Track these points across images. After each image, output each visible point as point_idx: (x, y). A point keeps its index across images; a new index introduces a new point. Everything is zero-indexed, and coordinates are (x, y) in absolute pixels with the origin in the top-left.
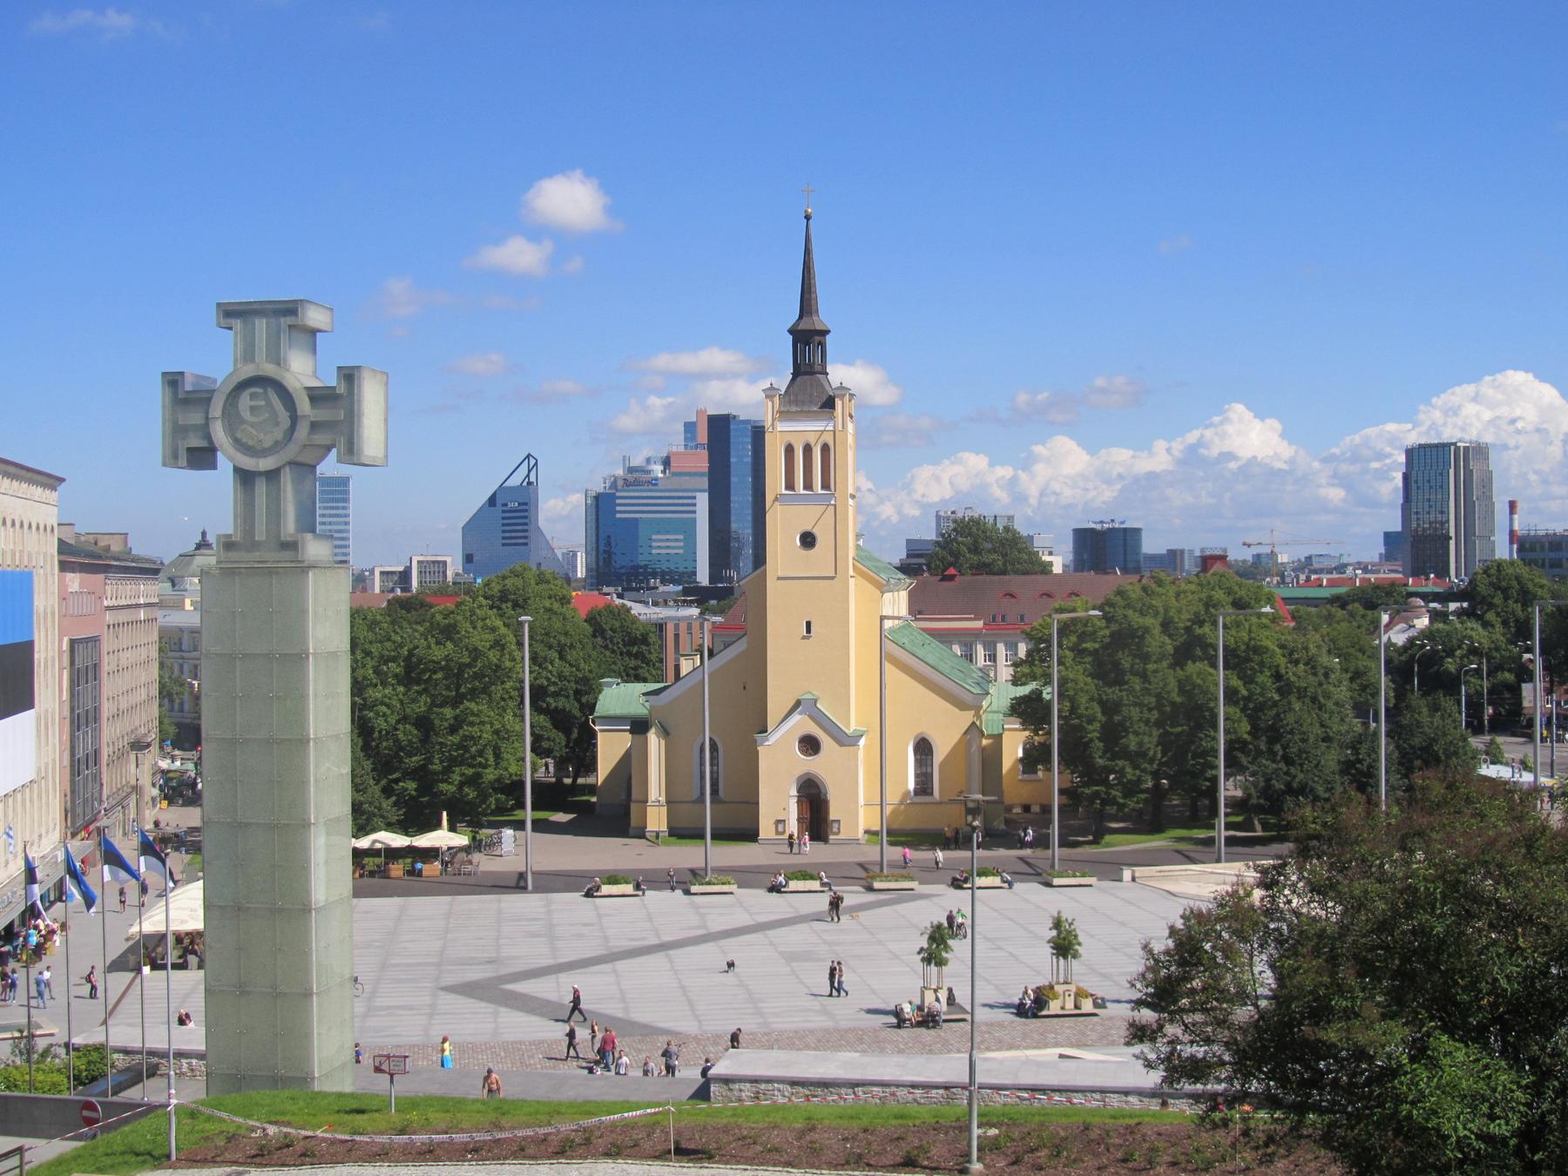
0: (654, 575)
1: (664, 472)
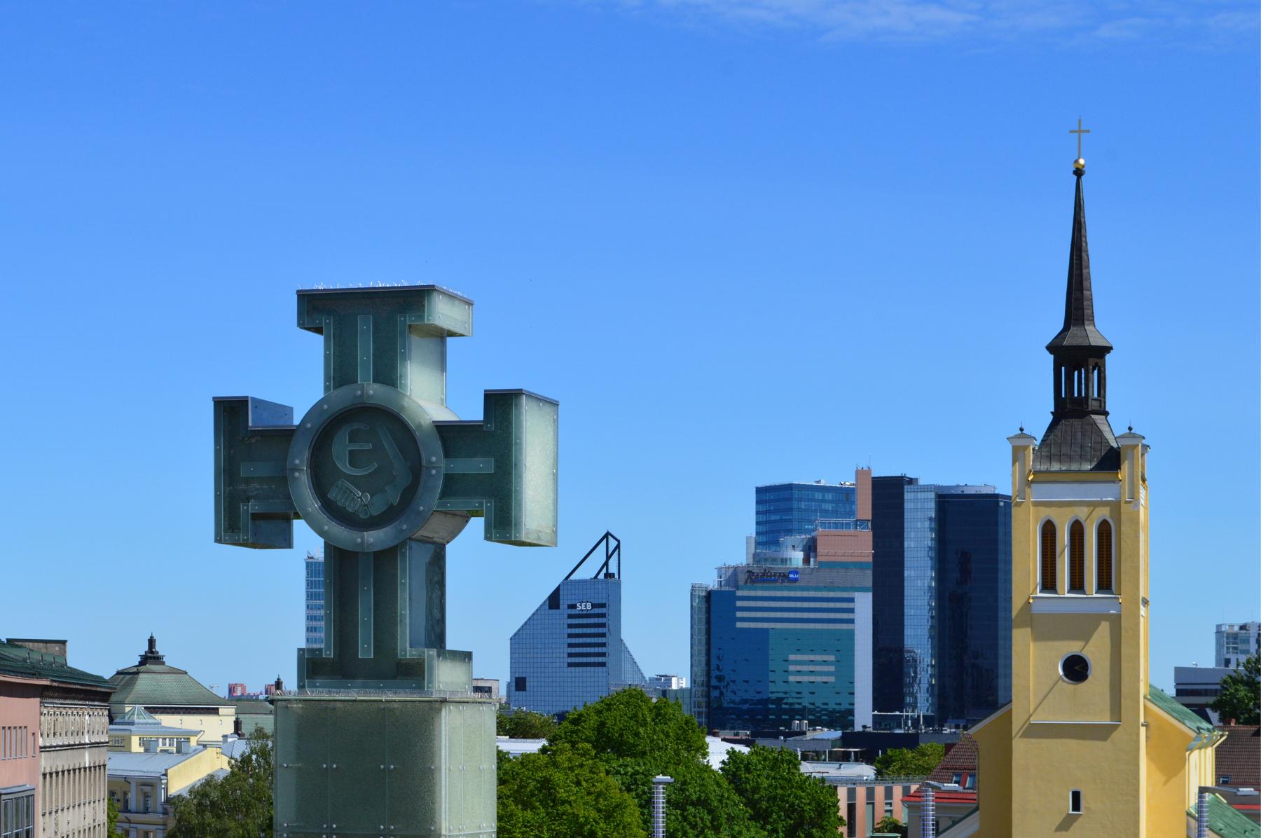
0: (802, 713)
1: (806, 560)
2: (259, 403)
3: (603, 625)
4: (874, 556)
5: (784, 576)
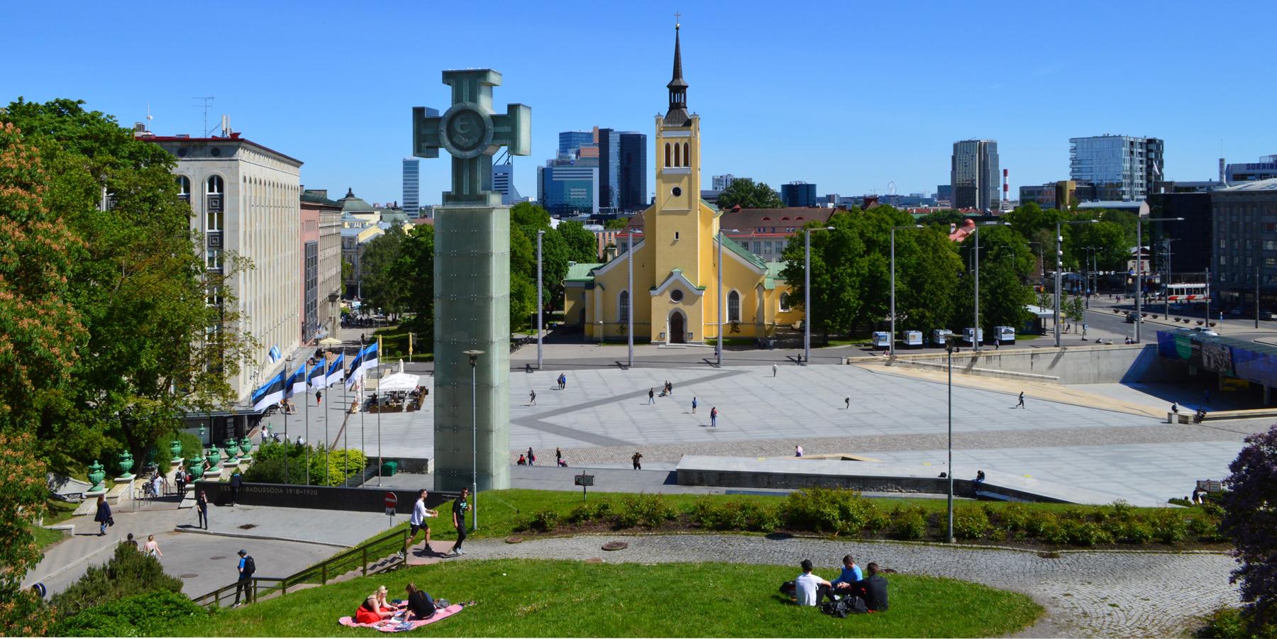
0: (576, 208)
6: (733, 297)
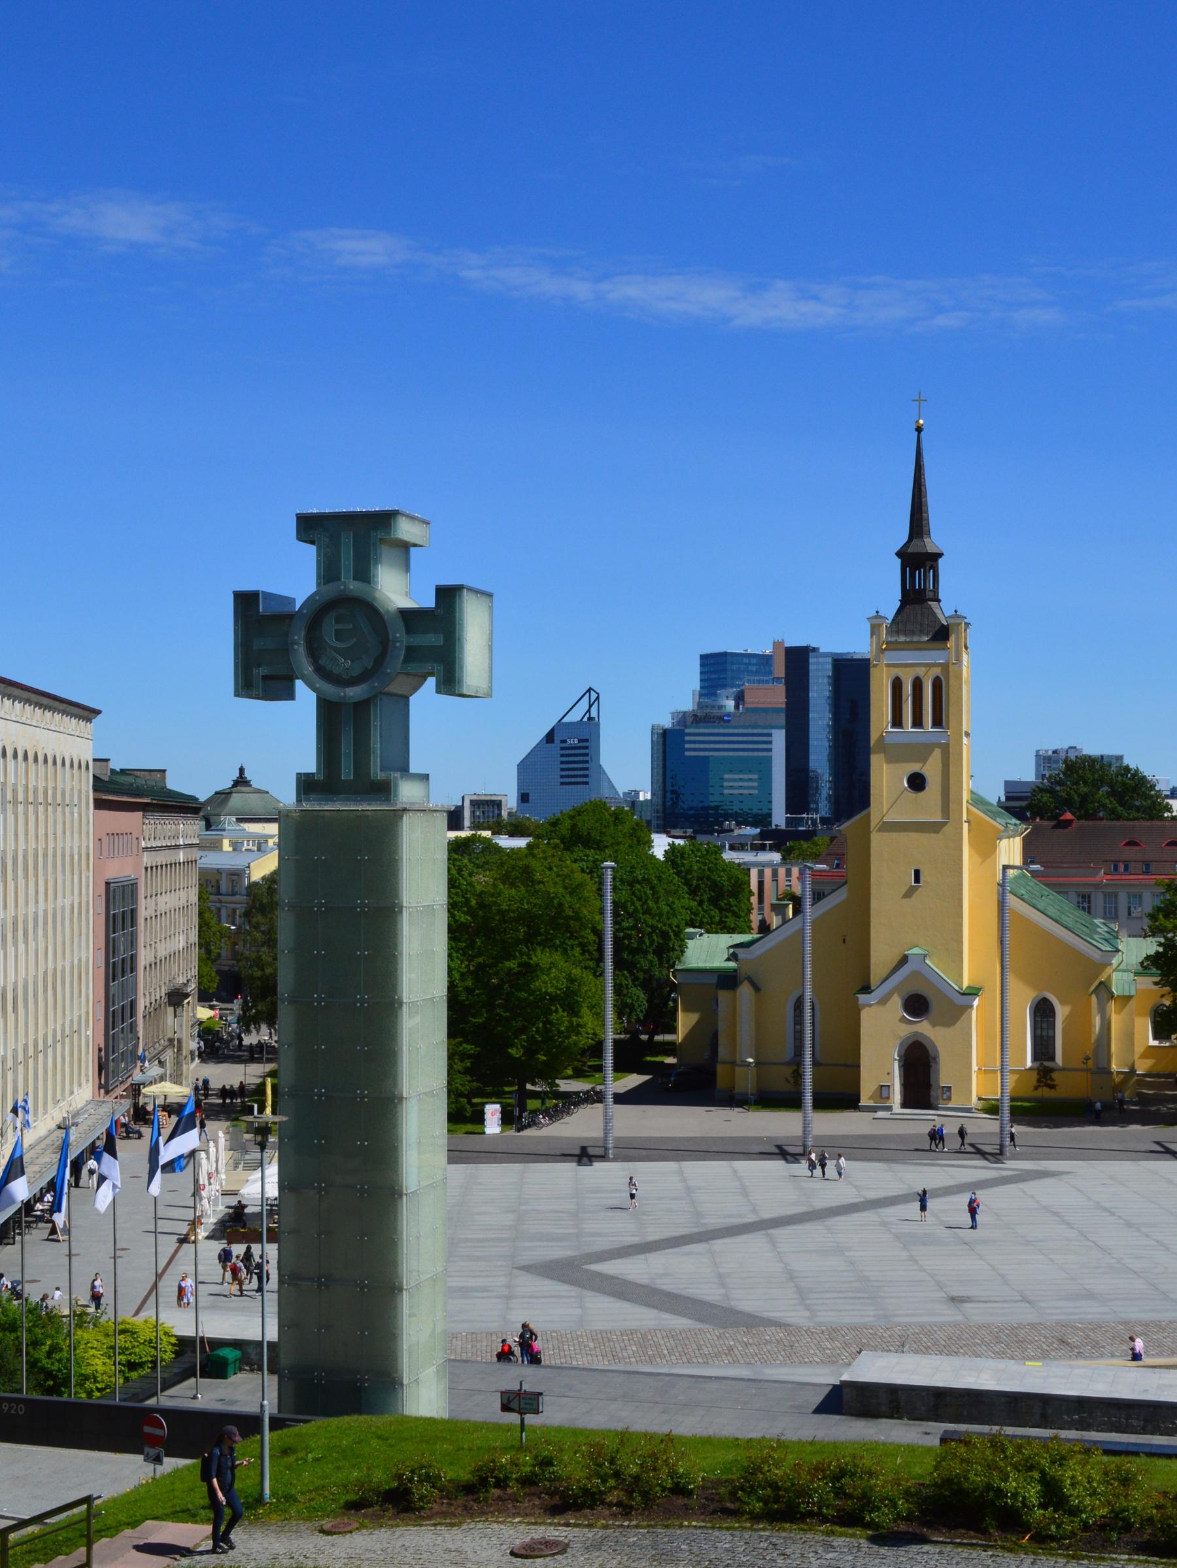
0: (727, 816)
1: (737, 707)
2: (268, 596)
3: (587, 755)
4: (787, 703)
5: (721, 719)
6: (1043, 1011)
